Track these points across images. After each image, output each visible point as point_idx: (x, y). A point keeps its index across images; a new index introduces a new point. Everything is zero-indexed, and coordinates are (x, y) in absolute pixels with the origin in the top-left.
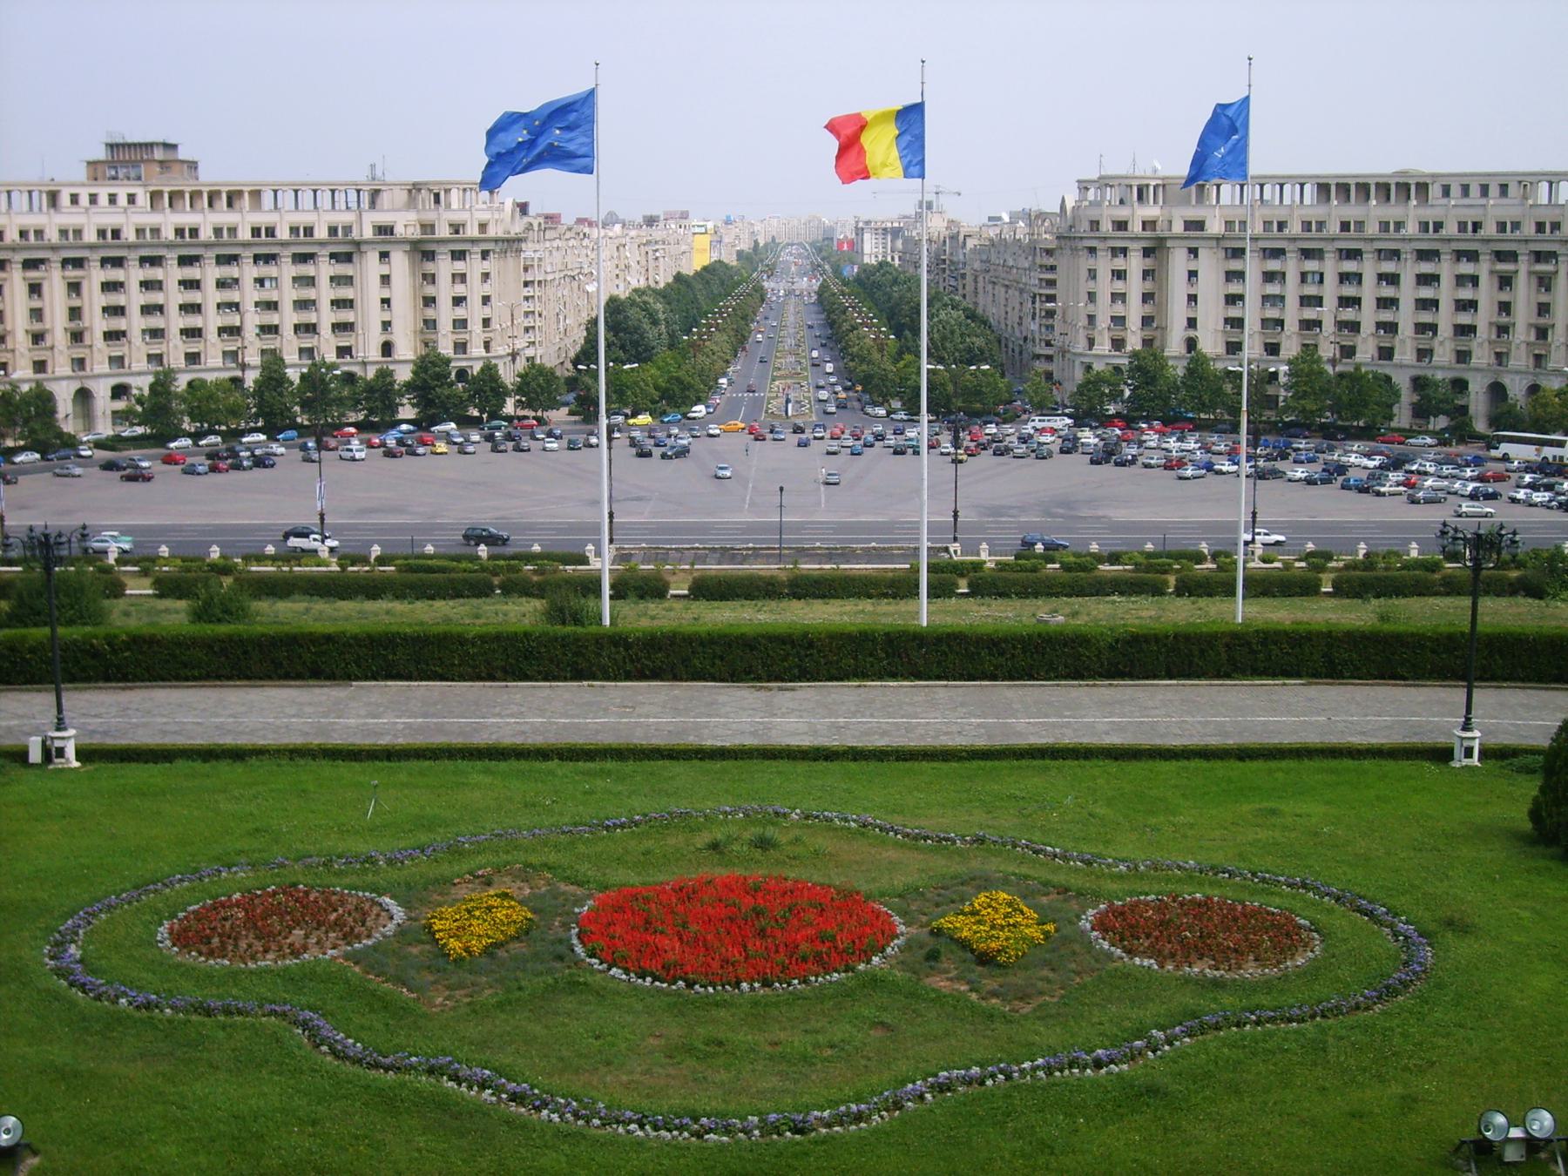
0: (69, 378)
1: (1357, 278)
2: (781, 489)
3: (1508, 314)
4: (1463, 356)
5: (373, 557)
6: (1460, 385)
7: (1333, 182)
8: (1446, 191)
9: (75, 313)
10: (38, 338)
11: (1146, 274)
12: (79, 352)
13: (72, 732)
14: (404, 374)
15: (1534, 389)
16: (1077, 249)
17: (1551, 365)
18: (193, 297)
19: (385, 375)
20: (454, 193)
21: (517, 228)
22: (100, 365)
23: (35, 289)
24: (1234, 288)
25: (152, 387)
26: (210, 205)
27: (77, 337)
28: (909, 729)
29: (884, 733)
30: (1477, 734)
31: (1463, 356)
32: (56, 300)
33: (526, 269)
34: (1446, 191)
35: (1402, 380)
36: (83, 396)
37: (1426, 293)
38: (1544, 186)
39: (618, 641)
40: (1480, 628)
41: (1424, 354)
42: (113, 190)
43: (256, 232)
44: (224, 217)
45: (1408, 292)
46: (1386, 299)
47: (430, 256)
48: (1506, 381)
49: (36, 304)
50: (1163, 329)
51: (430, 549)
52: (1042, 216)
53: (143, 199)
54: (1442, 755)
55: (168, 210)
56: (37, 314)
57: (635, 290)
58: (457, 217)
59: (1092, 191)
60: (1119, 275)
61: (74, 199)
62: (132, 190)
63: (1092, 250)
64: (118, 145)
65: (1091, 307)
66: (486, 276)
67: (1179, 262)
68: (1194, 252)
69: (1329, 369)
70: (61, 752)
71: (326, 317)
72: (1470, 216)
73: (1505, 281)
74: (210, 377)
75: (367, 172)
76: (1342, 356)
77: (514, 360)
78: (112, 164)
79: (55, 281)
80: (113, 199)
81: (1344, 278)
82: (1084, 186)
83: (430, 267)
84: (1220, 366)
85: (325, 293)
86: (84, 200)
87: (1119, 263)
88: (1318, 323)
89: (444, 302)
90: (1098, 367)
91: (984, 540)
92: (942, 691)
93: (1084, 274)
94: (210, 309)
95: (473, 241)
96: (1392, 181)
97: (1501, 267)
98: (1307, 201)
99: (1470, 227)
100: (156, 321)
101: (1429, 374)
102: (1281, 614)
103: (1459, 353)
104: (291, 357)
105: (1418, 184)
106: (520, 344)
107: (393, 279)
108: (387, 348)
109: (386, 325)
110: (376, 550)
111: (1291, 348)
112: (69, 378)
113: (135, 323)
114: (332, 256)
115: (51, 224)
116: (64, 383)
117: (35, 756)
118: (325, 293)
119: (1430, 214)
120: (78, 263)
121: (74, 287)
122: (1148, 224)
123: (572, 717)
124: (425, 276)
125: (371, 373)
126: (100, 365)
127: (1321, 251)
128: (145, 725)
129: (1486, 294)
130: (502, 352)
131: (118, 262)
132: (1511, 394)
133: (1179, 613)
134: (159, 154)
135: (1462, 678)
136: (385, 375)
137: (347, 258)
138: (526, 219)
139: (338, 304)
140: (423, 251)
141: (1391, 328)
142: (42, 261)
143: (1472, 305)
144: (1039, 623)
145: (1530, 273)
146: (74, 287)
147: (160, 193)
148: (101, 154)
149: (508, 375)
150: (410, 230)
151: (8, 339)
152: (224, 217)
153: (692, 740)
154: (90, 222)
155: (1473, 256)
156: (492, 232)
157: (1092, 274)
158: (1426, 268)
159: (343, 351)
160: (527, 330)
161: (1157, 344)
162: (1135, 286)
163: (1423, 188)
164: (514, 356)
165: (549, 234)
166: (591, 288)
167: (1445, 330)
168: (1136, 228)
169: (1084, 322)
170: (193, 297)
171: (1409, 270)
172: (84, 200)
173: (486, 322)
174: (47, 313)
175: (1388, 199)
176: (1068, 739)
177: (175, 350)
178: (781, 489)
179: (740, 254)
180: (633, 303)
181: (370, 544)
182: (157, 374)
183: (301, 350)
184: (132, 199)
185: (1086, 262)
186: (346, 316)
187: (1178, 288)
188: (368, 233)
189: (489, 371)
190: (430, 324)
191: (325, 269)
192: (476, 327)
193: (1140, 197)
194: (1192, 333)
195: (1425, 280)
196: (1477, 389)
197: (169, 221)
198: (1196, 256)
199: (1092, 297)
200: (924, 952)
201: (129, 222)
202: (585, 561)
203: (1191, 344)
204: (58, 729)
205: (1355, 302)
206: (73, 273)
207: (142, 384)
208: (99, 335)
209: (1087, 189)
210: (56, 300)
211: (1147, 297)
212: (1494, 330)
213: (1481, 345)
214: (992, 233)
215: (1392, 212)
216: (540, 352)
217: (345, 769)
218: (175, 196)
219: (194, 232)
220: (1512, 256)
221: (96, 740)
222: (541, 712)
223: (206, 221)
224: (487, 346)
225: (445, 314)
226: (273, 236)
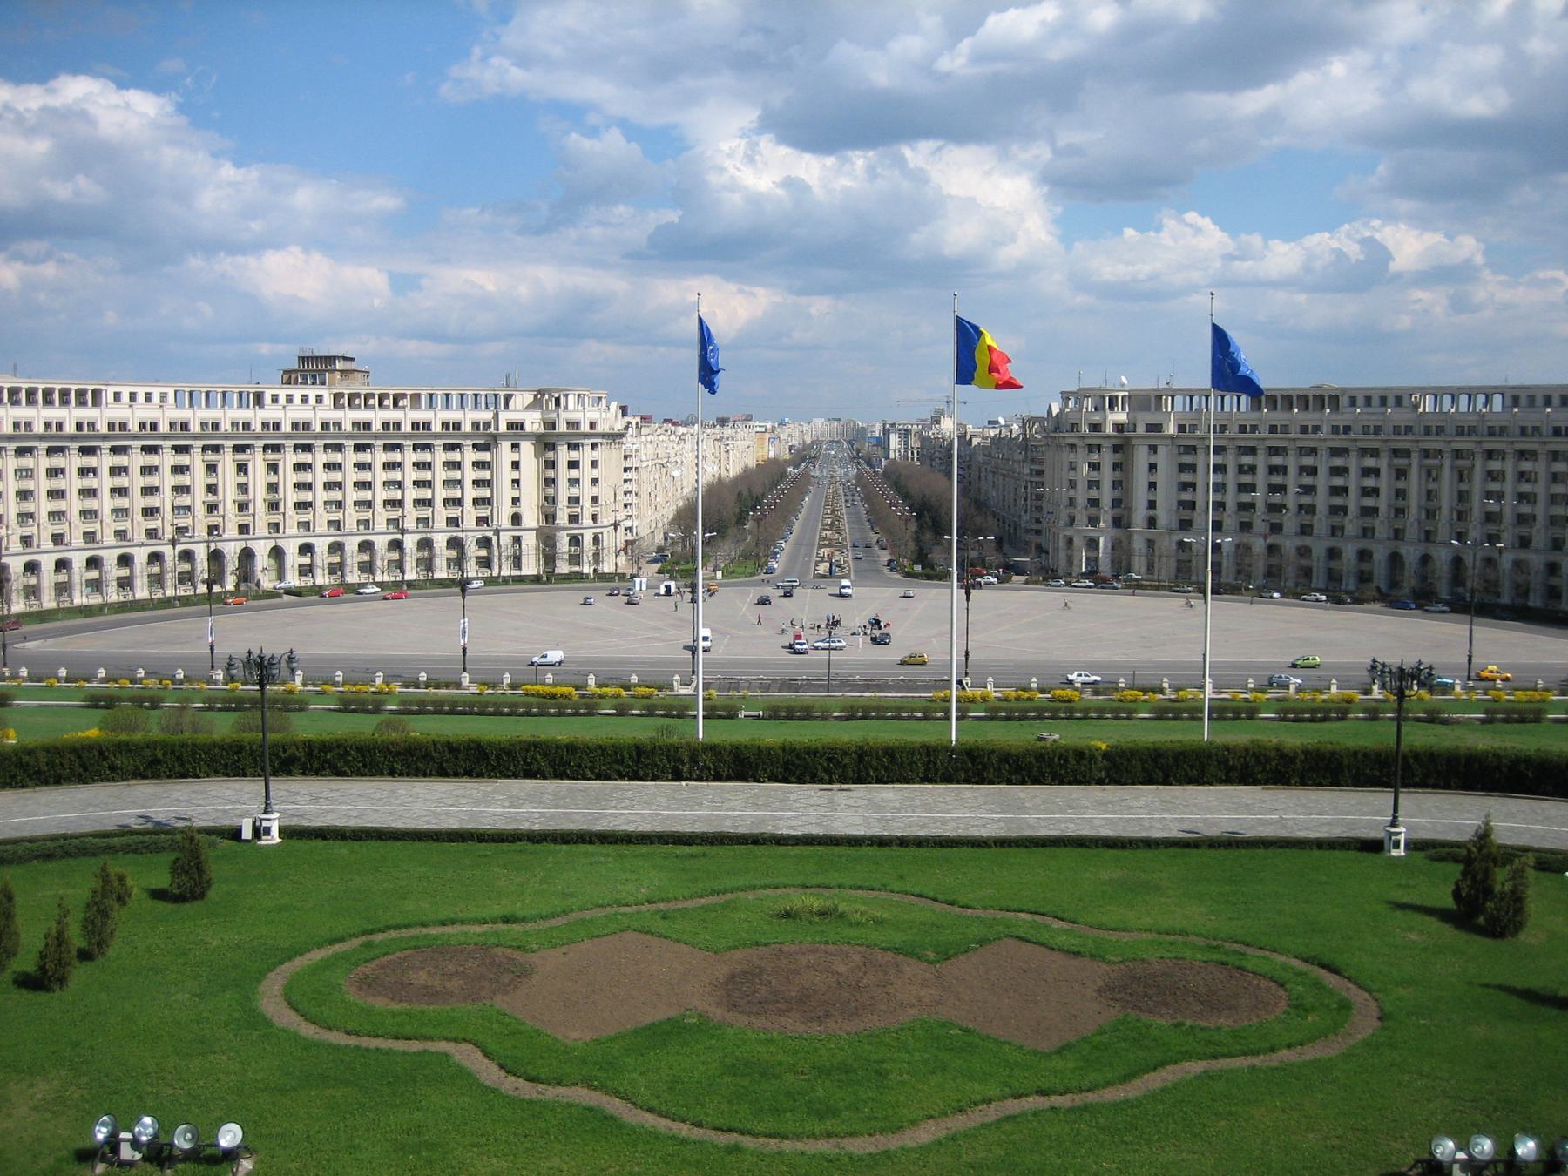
1: (1252, 469)
9: (273, 487)
10: (243, 506)
11: (1116, 466)
12: (275, 518)
13: (276, 815)
21: (619, 426)
22: (291, 528)
23: (242, 468)
24: (1186, 477)
27: (273, 506)
28: (943, 822)
29: (923, 826)
30: (1402, 829)
32: (259, 477)
36: (277, 553)
37: (1338, 482)
38: (1429, 399)
39: (712, 749)
40: (1403, 746)
42: (290, 392)
46: (1245, 485)
47: (551, 446)
48: (1403, 551)
50: (1129, 509)
52: (1035, 420)
53: (328, 399)
54: (1374, 846)
56: (243, 488)
58: (574, 416)
62: (319, 392)
63: (1072, 447)
65: (1072, 492)
67: (1141, 458)
70: (267, 831)
79: (257, 462)
80: (304, 399)
81: (1241, 470)
82: (1066, 397)
88: (1252, 505)
89: (562, 483)
92: (970, 792)
93: (1066, 466)
95: (586, 436)
98: (1243, 408)
102: (1238, 736)
103: (1365, 530)
109: (515, 501)
114: (474, 446)
115: (256, 417)
117: (247, 833)
119: (1340, 420)
120: (277, 449)
121: (273, 468)
126: (291, 528)
127: (191, 447)
128: (332, 811)
130: (606, 523)
131: (307, 448)
134: (339, 365)
135: (1387, 785)
138: (627, 419)
140: (546, 443)
142: (248, 447)
143: (1282, 489)
146: (273, 468)
147: (341, 395)
150: (536, 426)
153: (770, 829)
155: (1375, 453)
156: (600, 429)
157: (1072, 467)
158: (1338, 462)
162: (1107, 476)
165: (645, 431)
166: (676, 474)
171: (1324, 463)
173: (595, 499)
176: (1072, 830)
181: (1119, 676)
184: (319, 399)
187: (1141, 477)
188: (503, 428)
192: (586, 502)
194: (1152, 512)
195: (1337, 471)
197: (348, 417)
199: (1072, 484)
201: (318, 416)
202: (458, 685)
204: (266, 812)
205: (1282, 489)
206: (271, 456)
208: (290, 505)
210: (259, 477)
211: (1116, 484)
214: (993, 433)
215: (1310, 418)
217: (342, 849)
220: (1407, 453)
221: (295, 822)
222: (648, 804)
223: (377, 417)
225: (563, 492)
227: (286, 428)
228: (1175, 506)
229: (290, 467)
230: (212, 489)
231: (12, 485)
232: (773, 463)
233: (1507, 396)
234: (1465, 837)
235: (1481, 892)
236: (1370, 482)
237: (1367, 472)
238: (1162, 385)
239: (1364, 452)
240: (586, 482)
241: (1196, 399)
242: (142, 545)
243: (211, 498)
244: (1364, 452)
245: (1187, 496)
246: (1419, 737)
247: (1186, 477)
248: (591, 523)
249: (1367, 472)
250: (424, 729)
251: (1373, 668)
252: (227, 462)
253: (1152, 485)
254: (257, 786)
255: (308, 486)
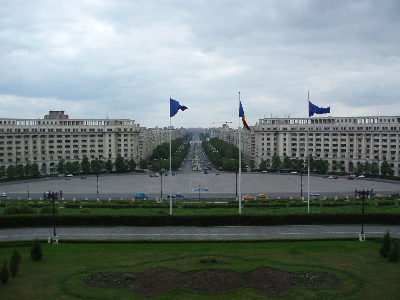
0: (41, 161)
2: (200, 186)
3: (353, 147)
4: (343, 156)
5: (109, 200)
6: (343, 162)
7: (314, 119)
8: (338, 121)
9: (43, 147)
11: (275, 139)
14: (114, 161)
15: (359, 163)
16: (259, 134)
17: (362, 158)
18: (68, 144)
19: (109, 161)
20: (125, 122)
23: (35, 142)
24: (294, 142)
25: (59, 163)
26: (72, 124)
27: (43, 152)
31: (343, 156)
33: (140, 139)
34: (338, 121)
35: (330, 161)
37: (335, 143)
41: (335, 156)
43: (82, 130)
44: (75, 127)
45: (331, 143)
47: (120, 135)
48: (353, 161)
49: (35, 145)
51: (122, 199)
53: (58, 123)
55: (64, 125)
56: (35, 147)
57: (163, 143)
58: (125, 127)
59: (262, 122)
60: (269, 139)
61: (44, 123)
63: (263, 134)
64: (51, 111)
65: (263, 146)
66: (132, 140)
67: (281, 136)
68: (285, 134)
69: (315, 159)
70: (55, 241)
71: (96, 148)
72: (344, 126)
73: (368, 140)
74: (72, 161)
75: (106, 117)
76: (317, 156)
77: (138, 158)
78: (50, 115)
80: (52, 123)
82: (261, 121)
83: (119, 138)
84: (291, 159)
85: (96, 143)
86: (46, 123)
87: (269, 137)
88: (304, 149)
90: (265, 159)
91: (291, 196)
93: (261, 139)
94: (72, 146)
96: (327, 119)
97: (367, 137)
99: (344, 129)
100: (60, 149)
101: (336, 160)
104: (89, 157)
105: (332, 120)
106: (139, 155)
107: (112, 141)
108: (110, 155)
110: (110, 199)
111: (306, 154)
112: (41, 161)
113: (55, 149)
116: (40, 162)
117: (49, 242)
118: (96, 143)
119: (335, 126)
120: (44, 136)
122: (275, 129)
123: (166, 234)
124: (118, 140)
125: (106, 161)
129: (347, 143)
132: (354, 165)
133: (293, 211)
136: (109, 161)
137: (101, 136)
139: (99, 146)
140: (118, 134)
141: (327, 150)
142: (36, 136)
144: (331, 214)
145: (365, 138)
146: (43, 142)
147: (62, 122)
148: (48, 113)
149: (136, 161)
150: (116, 130)
151: (29, 153)
152: (75, 127)
153: (193, 239)
154: (47, 128)
155: (344, 135)
157: (263, 139)
158: (335, 137)
159: (101, 156)
160: (140, 152)
161: (277, 154)
162: (272, 142)
163: (333, 120)
164: (138, 157)
166: (153, 143)
167: (331, 150)
168: (272, 129)
169: (261, 149)
170: (68, 144)
171: (331, 138)
172: (46, 123)
173: (132, 150)
174: (29, 148)
175: (326, 123)
177: (64, 156)
178: (200, 186)
179: (184, 135)
180: (163, 146)
181: (108, 198)
182: (60, 161)
183: (59, 157)
184: (56, 123)
185: (262, 137)
186: (101, 148)
188: (106, 130)
189: (132, 161)
190: (119, 150)
191: (96, 138)
192: (129, 151)
193: (273, 123)
195: (334, 140)
196: (346, 165)
197: (63, 128)
198: (285, 135)
199: (263, 144)
200: (297, 285)
203: (285, 154)
205: (319, 145)
206: (43, 139)
207: (57, 163)
208: (48, 152)
209: (261, 121)
212: (349, 150)
213: (347, 153)
215: (327, 125)
216: (143, 156)
218: (65, 122)
219: (69, 130)
220: (353, 135)
222: (159, 233)
223: (71, 128)
224: (132, 155)
225: (122, 148)
226: (86, 131)
227: (47, 131)
228: (291, 150)
229: (48, 142)
230: (26, 148)
231: (397, 144)
232: (180, 138)
233: (379, 119)
234: (382, 236)
235: (389, 251)
236: (343, 143)
237: (342, 140)
238: (287, 117)
239: (342, 134)
240: (265, 144)
241: (300, 121)
242: (8, 163)
243: (26, 150)
244: (342, 134)
245: (294, 147)
246: (368, 211)
247: (294, 142)
248: (131, 156)
249: (342, 140)
250: (94, 212)
251: (356, 191)
252: (31, 141)
253: (285, 144)
254: (52, 230)
255: (61, 146)
